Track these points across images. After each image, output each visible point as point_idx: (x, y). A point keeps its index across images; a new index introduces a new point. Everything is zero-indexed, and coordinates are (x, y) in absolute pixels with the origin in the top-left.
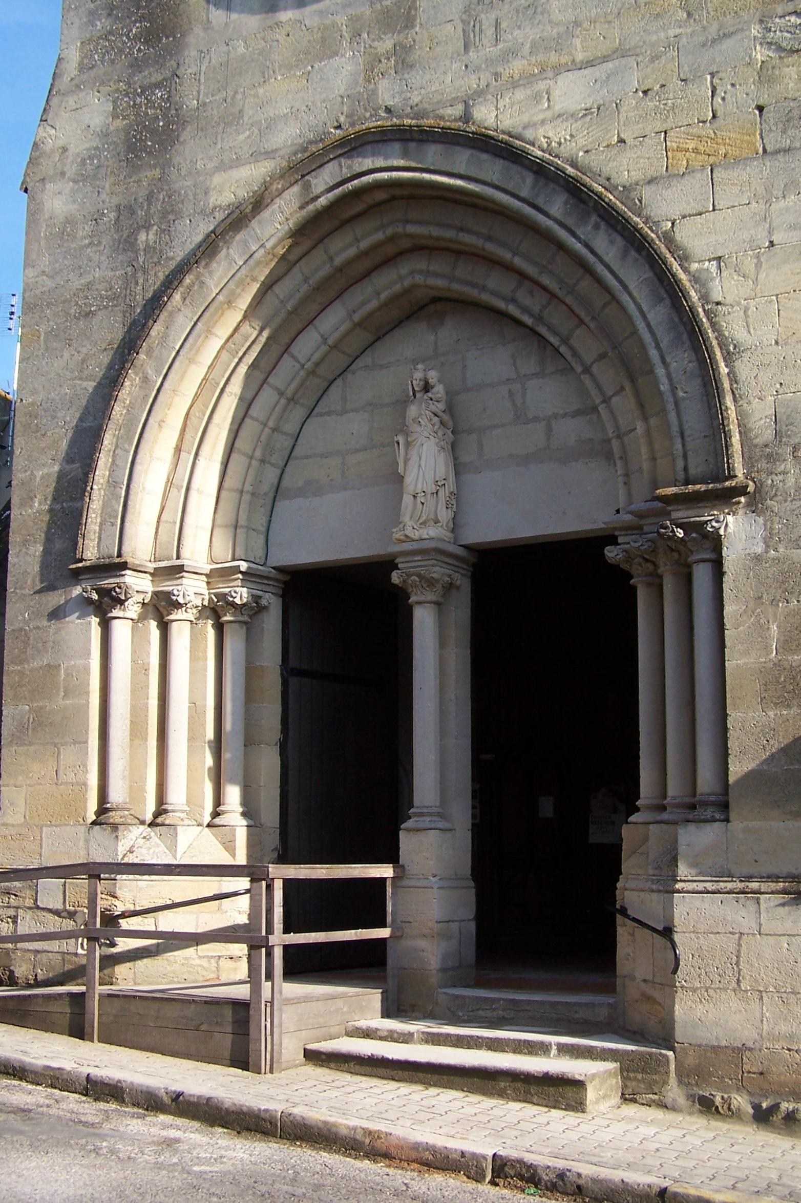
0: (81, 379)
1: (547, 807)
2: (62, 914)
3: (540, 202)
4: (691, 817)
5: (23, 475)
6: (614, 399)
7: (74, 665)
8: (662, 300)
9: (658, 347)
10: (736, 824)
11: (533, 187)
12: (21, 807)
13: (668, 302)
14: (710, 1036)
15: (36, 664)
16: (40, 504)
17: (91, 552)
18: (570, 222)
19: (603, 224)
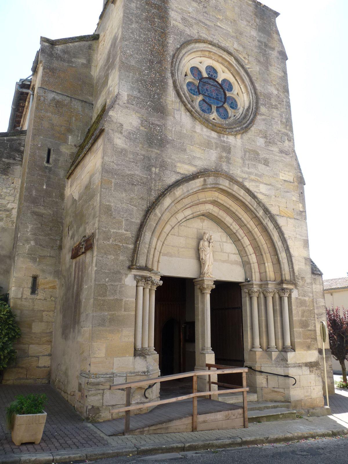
0: (130, 204)
1: (72, 462)
2: (125, 390)
3: (258, 210)
4: (272, 366)
5: (105, 229)
6: (252, 255)
7: (128, 300)
8: (280, 241)
9: (279, 250)
10: (297, 352)
11: (256, 206)
12: (104, 350)
13: (281, 242)
14: (297, 398)
15: (111, 298)
16: (112, 241)
17: (142, 262)
18: (264, 217)
19: (270, 220)
